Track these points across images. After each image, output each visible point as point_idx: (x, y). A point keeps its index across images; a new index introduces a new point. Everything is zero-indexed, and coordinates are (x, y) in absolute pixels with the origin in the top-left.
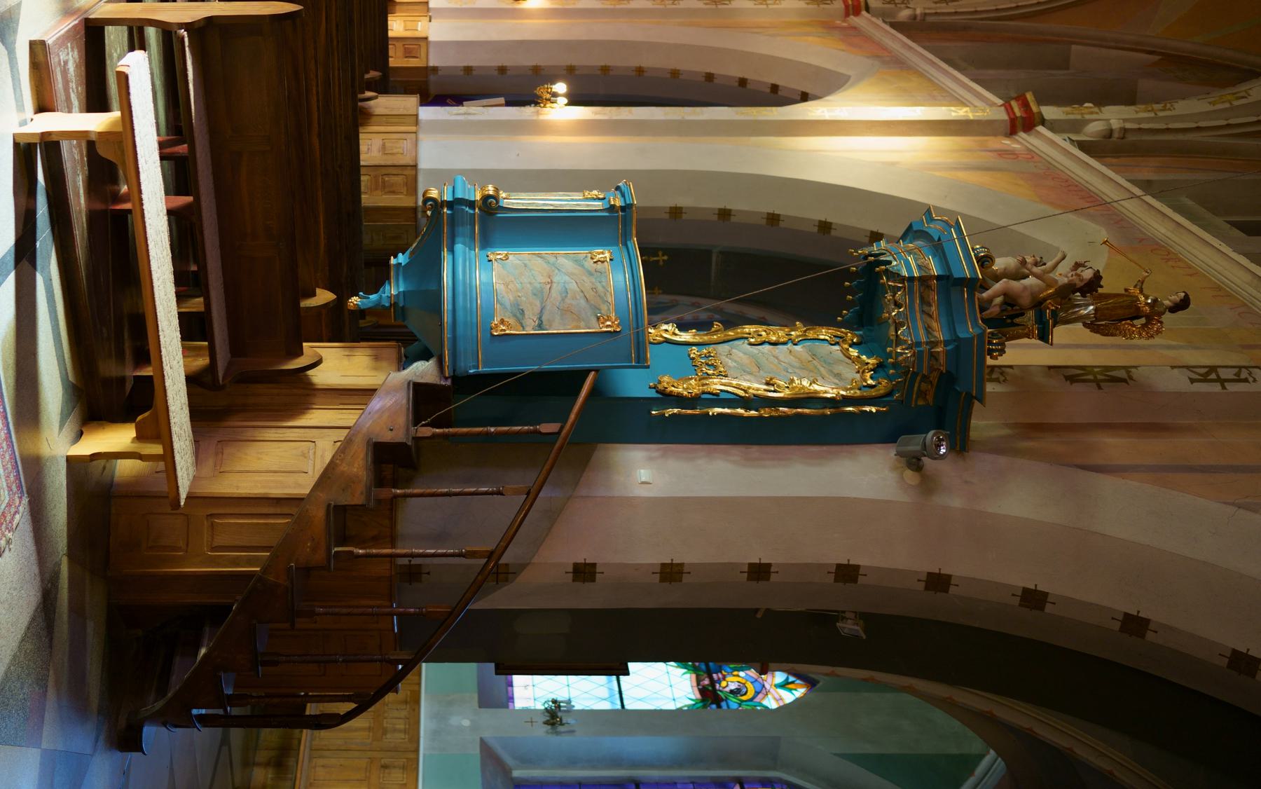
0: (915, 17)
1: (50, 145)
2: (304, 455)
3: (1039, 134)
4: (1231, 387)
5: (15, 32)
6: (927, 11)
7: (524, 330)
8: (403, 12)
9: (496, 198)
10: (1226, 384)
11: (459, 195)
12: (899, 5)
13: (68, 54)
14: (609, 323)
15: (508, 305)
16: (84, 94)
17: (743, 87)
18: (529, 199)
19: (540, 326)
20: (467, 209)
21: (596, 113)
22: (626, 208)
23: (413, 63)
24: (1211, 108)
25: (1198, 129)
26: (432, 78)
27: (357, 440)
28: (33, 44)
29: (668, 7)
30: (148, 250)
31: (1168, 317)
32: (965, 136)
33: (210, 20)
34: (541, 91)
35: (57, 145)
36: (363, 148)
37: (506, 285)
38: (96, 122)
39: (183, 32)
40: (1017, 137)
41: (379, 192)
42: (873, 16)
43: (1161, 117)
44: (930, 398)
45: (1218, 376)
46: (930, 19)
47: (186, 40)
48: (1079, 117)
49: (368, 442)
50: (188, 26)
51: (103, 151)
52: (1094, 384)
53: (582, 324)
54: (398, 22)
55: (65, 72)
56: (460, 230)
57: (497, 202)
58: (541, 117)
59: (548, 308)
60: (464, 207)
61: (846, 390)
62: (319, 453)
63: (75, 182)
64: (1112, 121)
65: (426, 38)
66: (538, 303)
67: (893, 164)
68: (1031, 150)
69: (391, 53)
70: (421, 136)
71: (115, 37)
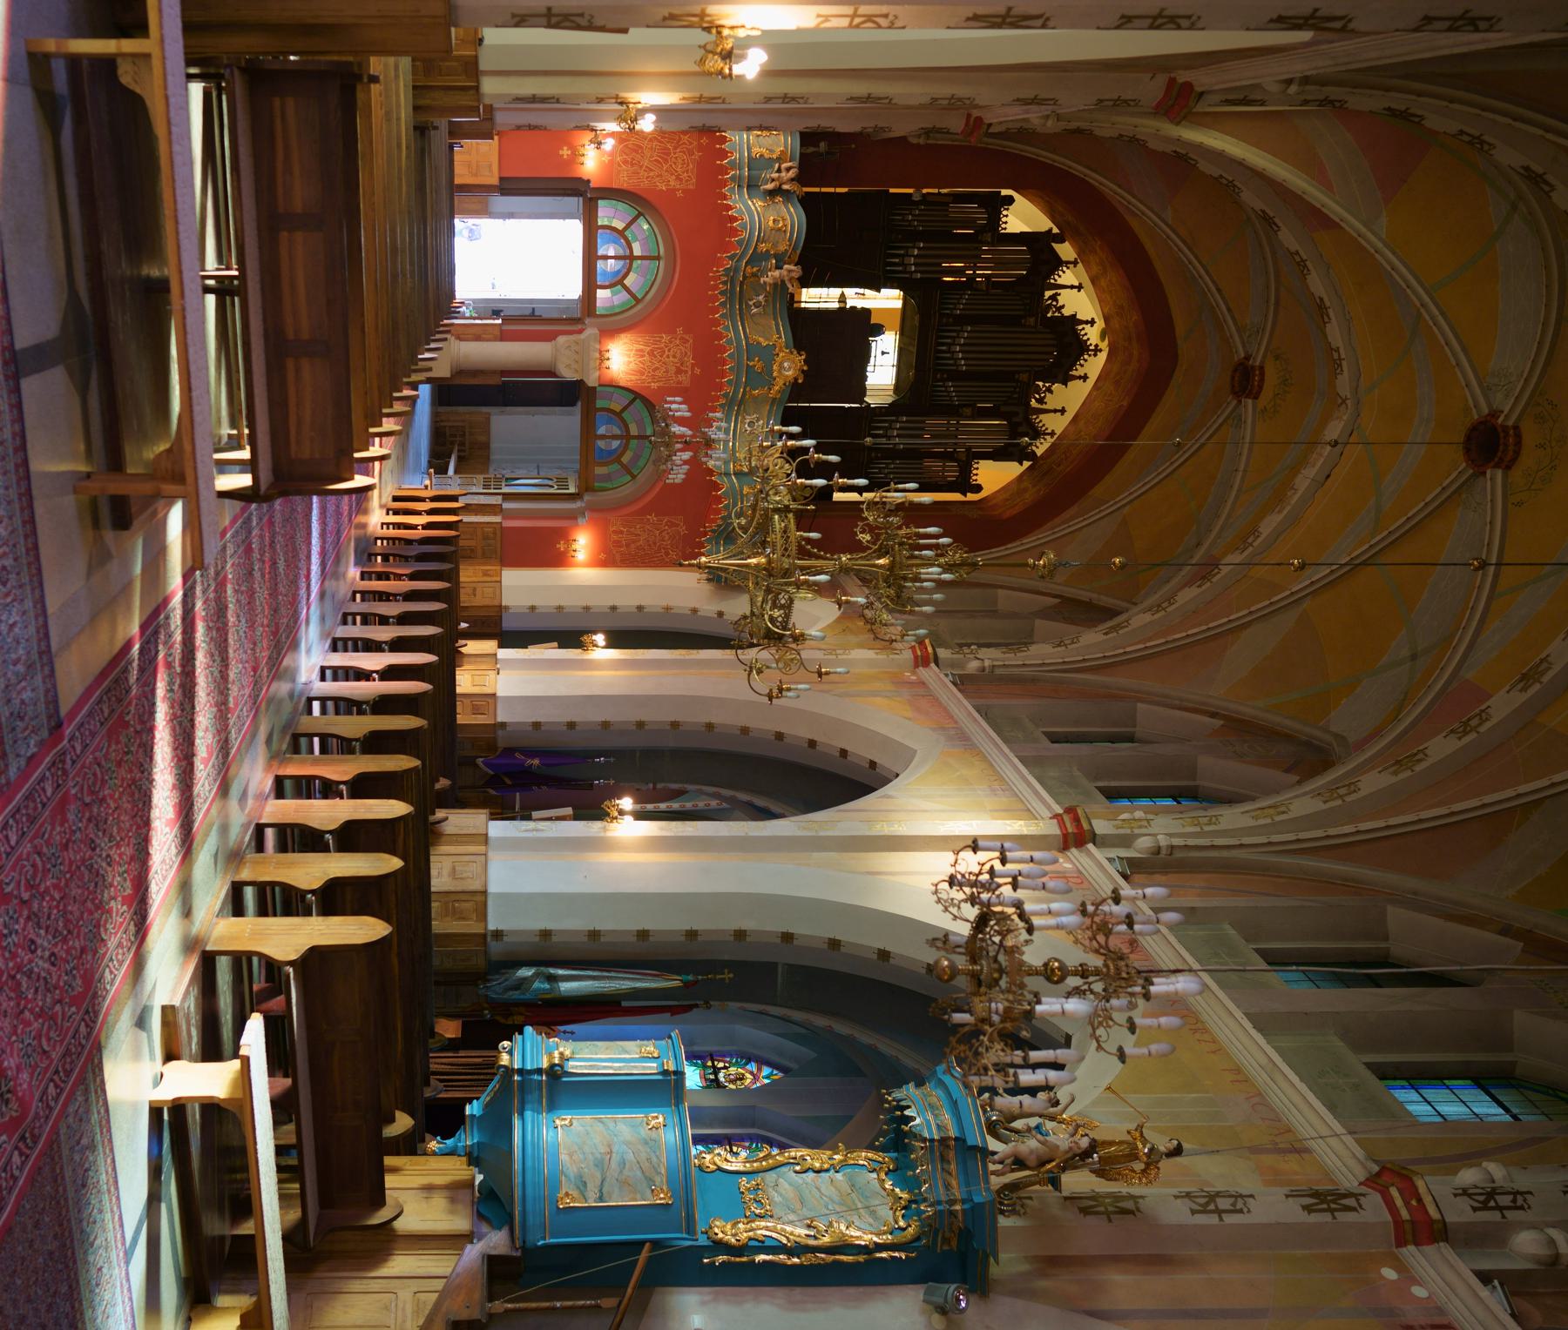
0: (983, 669)
1: (179, 1108)
2: (387, 1308)
3: (1089, 854)
4: (1229, 1219)
7: (586, 1202)
10: (1224, 1215)
12: (967, 656)
14: (662, 1196)
15: (572, 1176)
19: (601, 1199)
24: (1252, 823)
25: (1241, 846)
26: (500, 733)
28: (164, 1008)
30: (260, 1188)
31: (1165, 1164)
36: (434, 872)
37: (571, 1155)
40: (1069, 854)
41: (449, 919)
44: (954, 1244)
45: (1216, 1206)
46: (998, 671)
48: (1128, 831)
49: (447, 1322)
50: (291, 963)
52: (1105, 1217)
53: (638, 1196)
56: (529, 1098)
58: (609, 834)
59: (608, 1180)
61: (877, 1235)
62: (400, 1305)
64: (1159, 837)
65: (494, 695)
66: (598, 1175)
68: (1081, 873)
69: (459, 710)
70: (490, 854)
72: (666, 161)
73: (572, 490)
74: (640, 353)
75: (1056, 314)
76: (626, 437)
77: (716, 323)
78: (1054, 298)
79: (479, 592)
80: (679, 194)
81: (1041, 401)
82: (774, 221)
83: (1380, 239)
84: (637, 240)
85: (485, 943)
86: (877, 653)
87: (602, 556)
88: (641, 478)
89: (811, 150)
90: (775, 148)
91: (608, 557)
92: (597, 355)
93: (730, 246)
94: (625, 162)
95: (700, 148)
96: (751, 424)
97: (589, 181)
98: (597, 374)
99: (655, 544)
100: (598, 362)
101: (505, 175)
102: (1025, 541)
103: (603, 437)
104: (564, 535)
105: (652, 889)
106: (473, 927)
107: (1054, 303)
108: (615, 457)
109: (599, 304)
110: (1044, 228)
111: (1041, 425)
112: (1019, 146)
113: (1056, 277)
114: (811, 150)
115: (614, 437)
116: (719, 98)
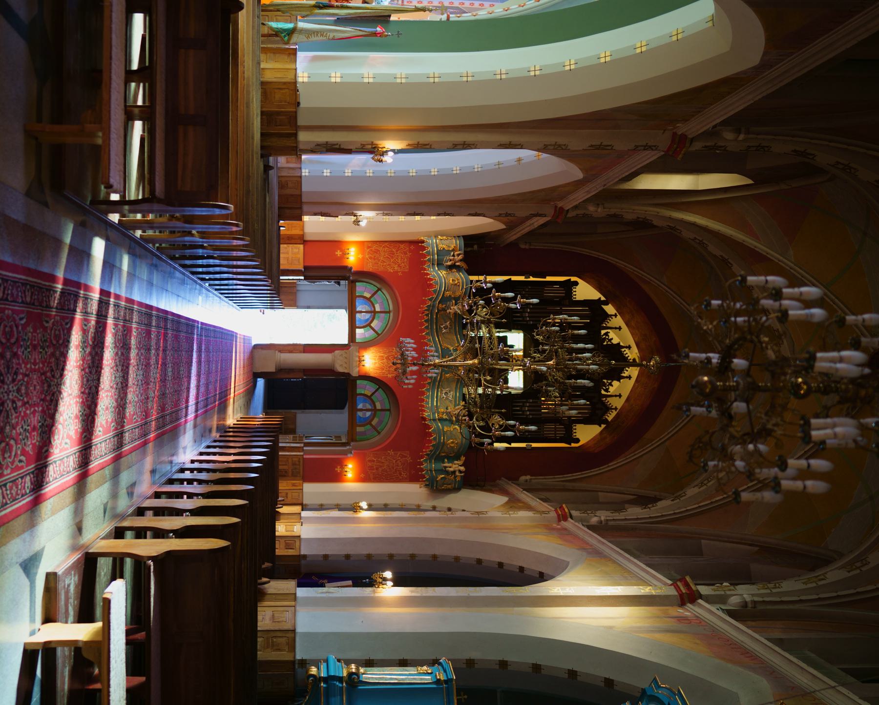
0: (601, 522)
1: (49, 649)
5: (37, 567)
6: (608, 518)
8: (285, 519)
9: (357, 674)
11: (332, 673)
13: (71, 579)
16: (78, 606)
17: (501, 568)
18: (380, 674)
20: (338, 683)
21: (412, 592)
22: (447, 681)
23: (291, 552)
24: (804, 587)
25: (801, 601)
26: (303, 562)
27: (152, 363)
28: (48, 575)
29: (449, 516)
32: (653, 606)
33: (169, 554)
34: (375, 576)
35: (54, 650)
36: (260, 618)
38: (83, 632)
39: (151, 563)
42: (576, 521)
43: (775, 593)
46: (611, 523)
47: (152, 568)
48: (723, 593)
50: (152, 558)
51: (85, 654)
54: (282, 526)
55: (67, 592)
57: (359, 677)
58: (377, 595)
60: (335, 682)
63: (63, 673)
65: (299, 536)
67: (611, 628)
69: (277, 546)
70: (298, 608)
71: (104, 566)
72: (392, 257)
73: (344, 441)
74: (381, 358)
75: (609, 343)
76: (374, 410)
77: (424, 337)
78: (607, 334)
79: (289, 496)
80: (400, 274)
81: (607, 390)
82: (453, 280)
83: (792, 262)
84: (377, 303)
85: (294, 669)
86: (534, 514)
87: (362, 475)
88: (383, 433)
89: (469, 249)
90: (450, 245)
91: (365, 476)
92: (357, 359)
93: (430, 293)
94: (370, 258)
95: (410, 251)
96: (446, 394)
97: (351, 268)
98: (358, 369)
99: (393, 468)
100: (358, 363)
101: (307, 264)
102: (610, 465)
103: (361, 410)
104: (341, 463)
105: (408, 629)
106: (285, 656)
107: (607, 337)
108: (368, 421)
109: (357, 336)
110: (596, 298)
111: (608, 404)
112: (579, 249)
113: (606, 323)
114: (469, 249)
115: (368, 410)
116: (428, 145)
